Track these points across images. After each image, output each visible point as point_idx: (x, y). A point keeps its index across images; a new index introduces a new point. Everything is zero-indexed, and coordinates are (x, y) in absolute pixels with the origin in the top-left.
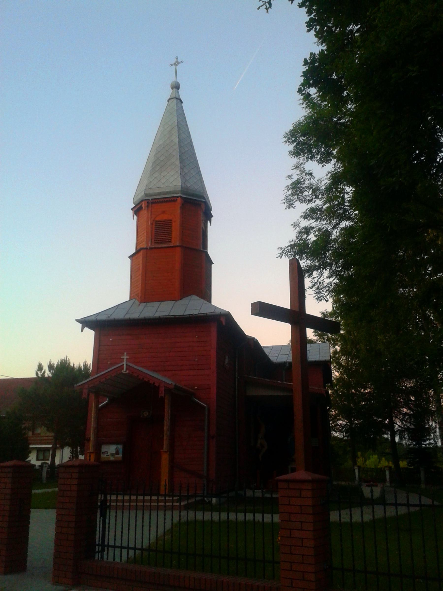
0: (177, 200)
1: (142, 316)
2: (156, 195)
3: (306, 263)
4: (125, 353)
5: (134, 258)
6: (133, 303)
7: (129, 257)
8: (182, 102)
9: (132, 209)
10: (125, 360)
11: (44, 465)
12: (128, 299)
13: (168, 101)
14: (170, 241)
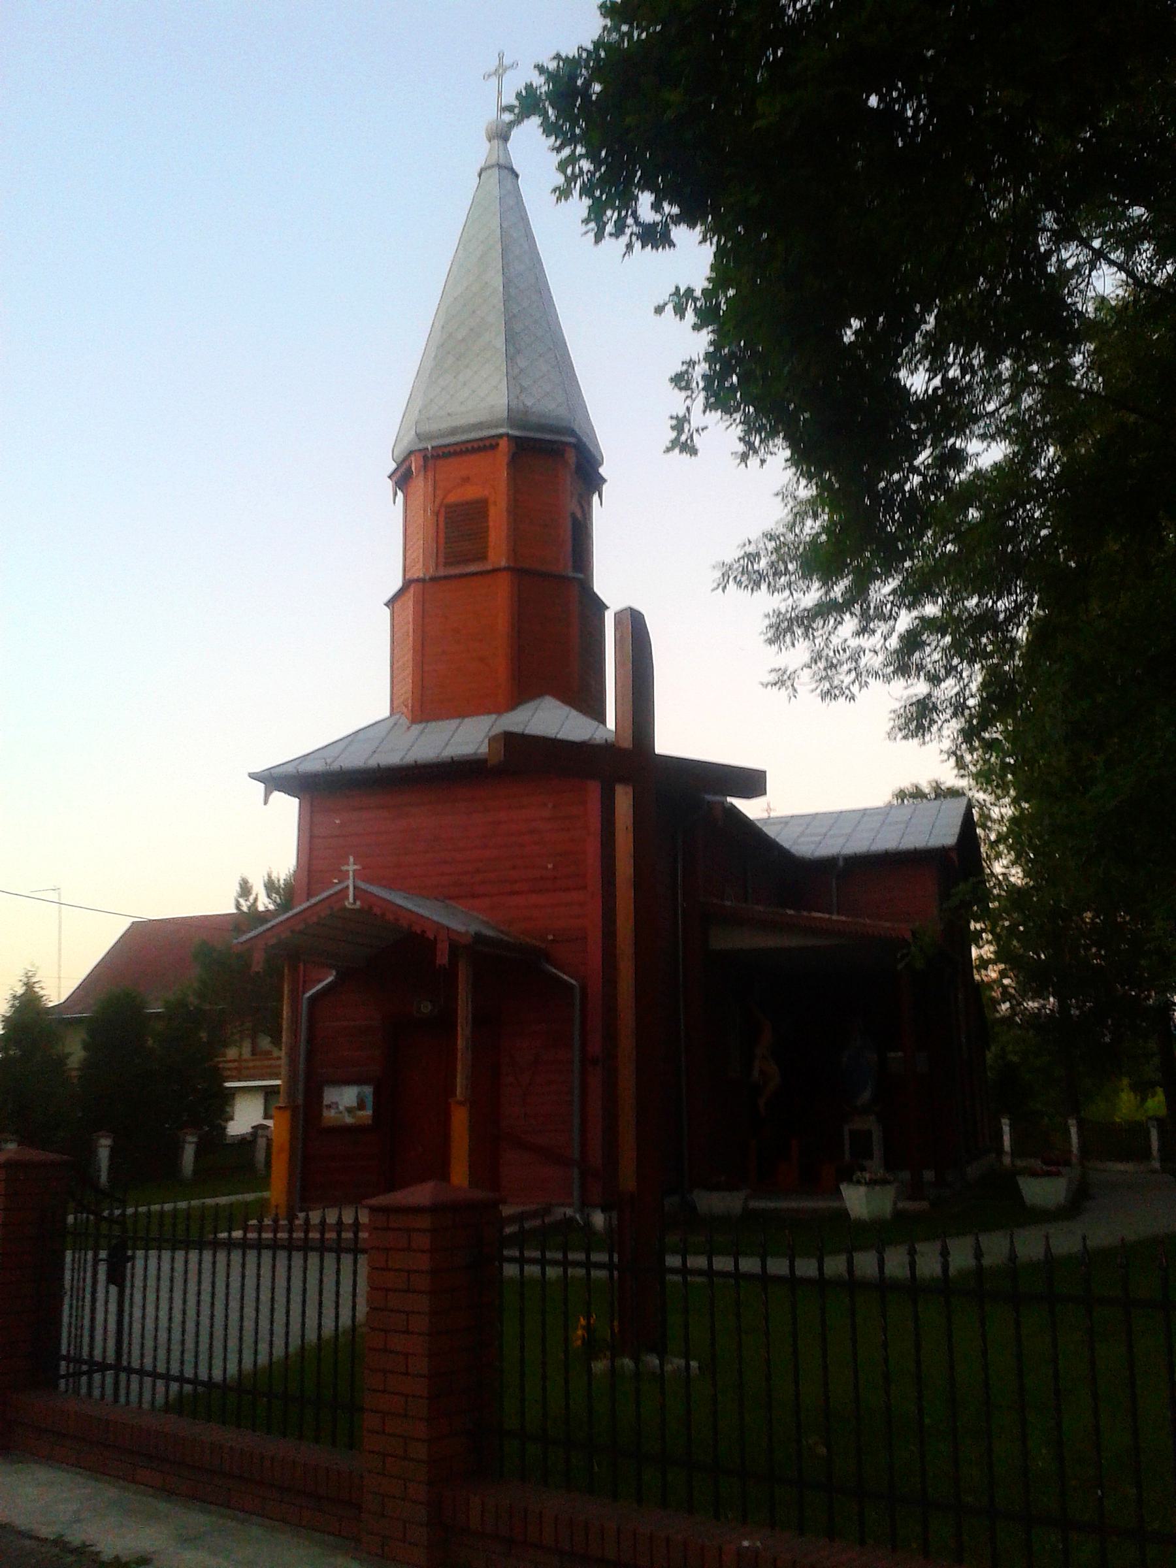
0: (498, 444)
1: (410, 759)
2: (497, 427)
3: (790, 600)
4: (351, 859)
5: (398, 605)
6: (395, 724)
7: (385, 605)
8: (517, 176)
9: (390, 477)
10: (351, 874)
11: (260, 1132)
12: (387, 713)
13: (480, 176)
14: (483, 557)
